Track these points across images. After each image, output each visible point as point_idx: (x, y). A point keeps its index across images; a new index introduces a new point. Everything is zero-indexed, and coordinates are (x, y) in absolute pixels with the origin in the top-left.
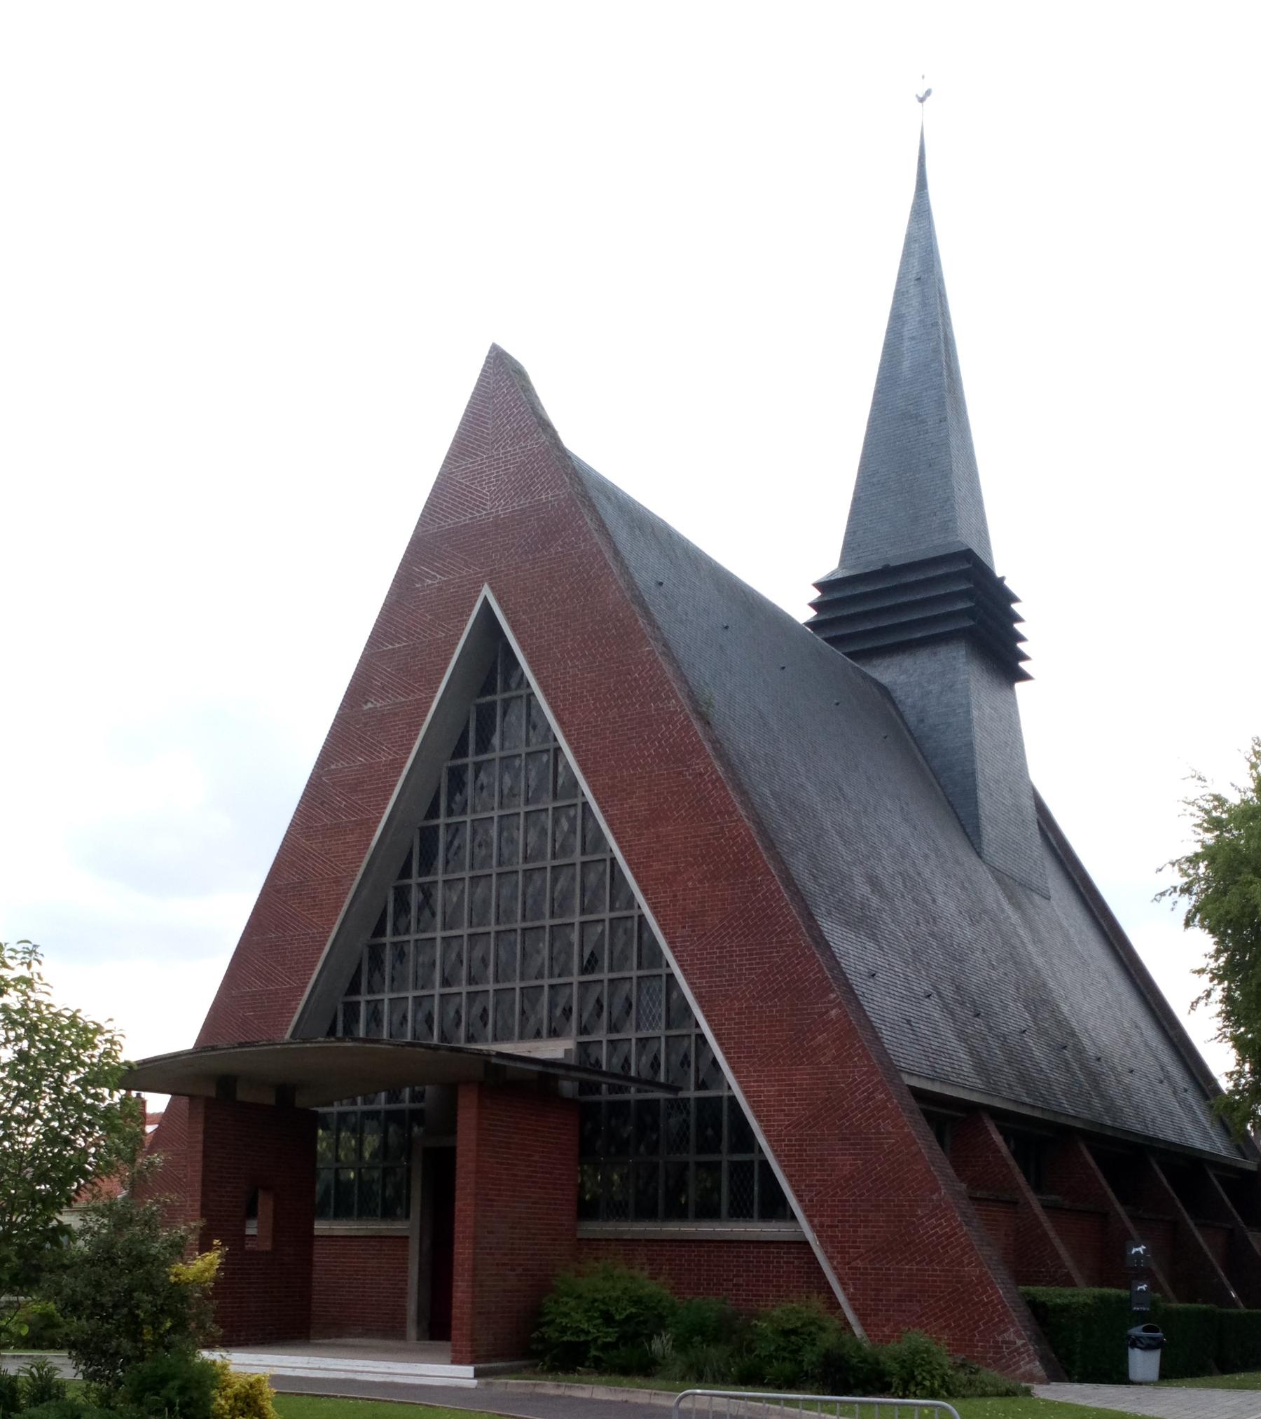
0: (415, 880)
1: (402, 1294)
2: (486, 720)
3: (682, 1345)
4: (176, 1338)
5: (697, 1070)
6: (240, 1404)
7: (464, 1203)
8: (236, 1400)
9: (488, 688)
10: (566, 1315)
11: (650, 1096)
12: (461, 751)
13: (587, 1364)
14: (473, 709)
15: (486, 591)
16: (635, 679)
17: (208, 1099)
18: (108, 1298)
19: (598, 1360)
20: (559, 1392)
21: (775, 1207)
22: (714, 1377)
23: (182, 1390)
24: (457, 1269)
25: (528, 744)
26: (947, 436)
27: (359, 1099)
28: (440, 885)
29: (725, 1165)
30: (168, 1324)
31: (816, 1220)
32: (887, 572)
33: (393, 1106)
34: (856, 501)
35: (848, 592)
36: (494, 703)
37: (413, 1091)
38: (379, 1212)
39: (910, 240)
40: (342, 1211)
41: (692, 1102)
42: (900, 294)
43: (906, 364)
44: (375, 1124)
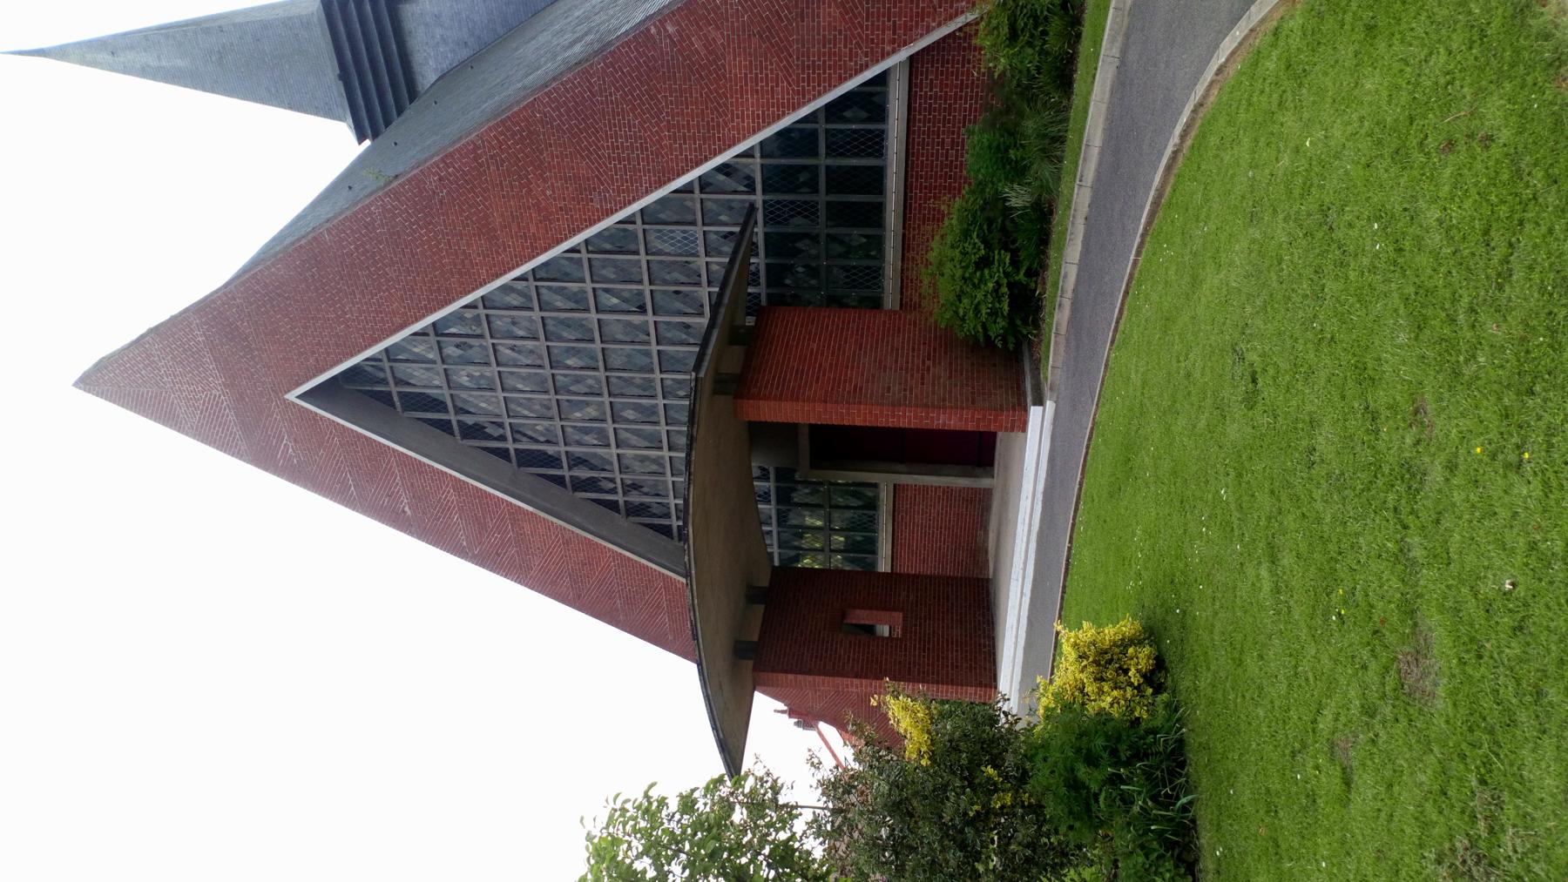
0: (565, 472)
1: (948, 491)
2: (421, 402)
3: (1018, 172)
4: (1010, 759)
5: (735, 192)
6: (1109, 674)
7: (858, 416)
8: (1102, 679)
9: (386, 398)
10: (977, 310)
11: (760, 241)
12: (445, 426)
13: (1033, 285)
14: (406, 414)
15: (292, 396)
16: (357, 248)
17: (755, 669)
18: (950, 856)
19: (1031, 273)
20: (1067, 303)
21: (870, 100)
22: (1061, 122)
23: (1092, 761)
24: (926, 424)
25: (434, 362)
26: (234, 25)
27: (766, 528)
28: (569, 449)
29: (830, 162)
30: (990, 770)
31: (888, 48)
32: (344, 76)
33: (773, 497)
34: (291, 107)
35: (364, 114)
36: (399, 393)
37: (758, 478)
38: (871, 513)
39: (83, 61)
40: (870, 546)
41: (768, 197)
42: (126, 70)
43: (180, 63)
44: (791, 515)
